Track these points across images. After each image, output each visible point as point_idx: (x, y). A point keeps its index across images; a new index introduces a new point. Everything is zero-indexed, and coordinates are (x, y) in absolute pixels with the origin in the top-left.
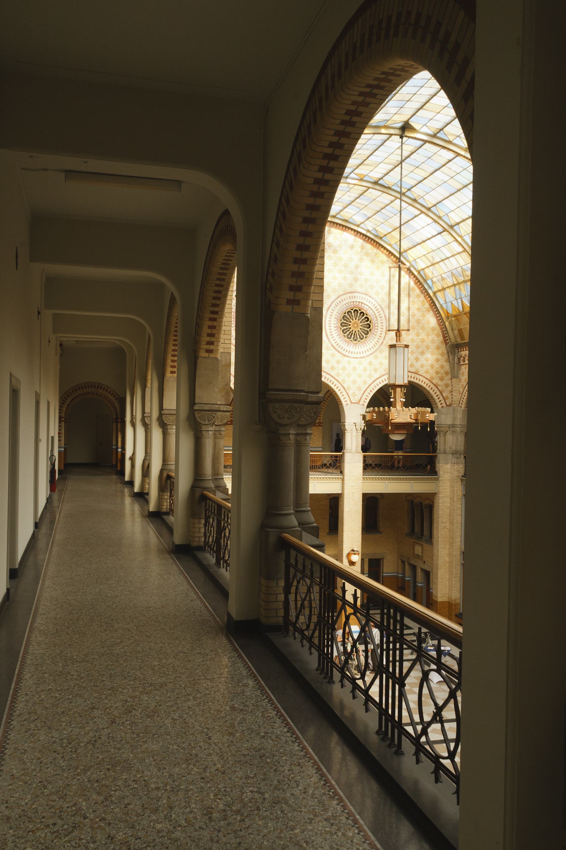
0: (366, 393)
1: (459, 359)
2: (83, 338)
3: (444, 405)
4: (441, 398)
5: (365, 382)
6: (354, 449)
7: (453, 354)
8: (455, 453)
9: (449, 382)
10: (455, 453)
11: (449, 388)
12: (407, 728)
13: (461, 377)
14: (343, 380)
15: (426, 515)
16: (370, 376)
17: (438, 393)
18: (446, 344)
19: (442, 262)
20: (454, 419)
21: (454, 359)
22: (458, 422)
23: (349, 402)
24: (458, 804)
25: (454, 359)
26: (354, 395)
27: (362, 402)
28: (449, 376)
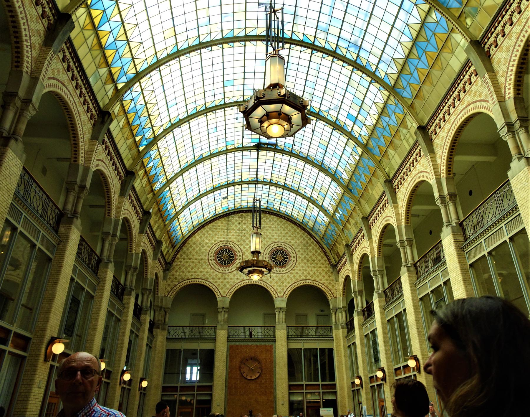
3: (332, 297)
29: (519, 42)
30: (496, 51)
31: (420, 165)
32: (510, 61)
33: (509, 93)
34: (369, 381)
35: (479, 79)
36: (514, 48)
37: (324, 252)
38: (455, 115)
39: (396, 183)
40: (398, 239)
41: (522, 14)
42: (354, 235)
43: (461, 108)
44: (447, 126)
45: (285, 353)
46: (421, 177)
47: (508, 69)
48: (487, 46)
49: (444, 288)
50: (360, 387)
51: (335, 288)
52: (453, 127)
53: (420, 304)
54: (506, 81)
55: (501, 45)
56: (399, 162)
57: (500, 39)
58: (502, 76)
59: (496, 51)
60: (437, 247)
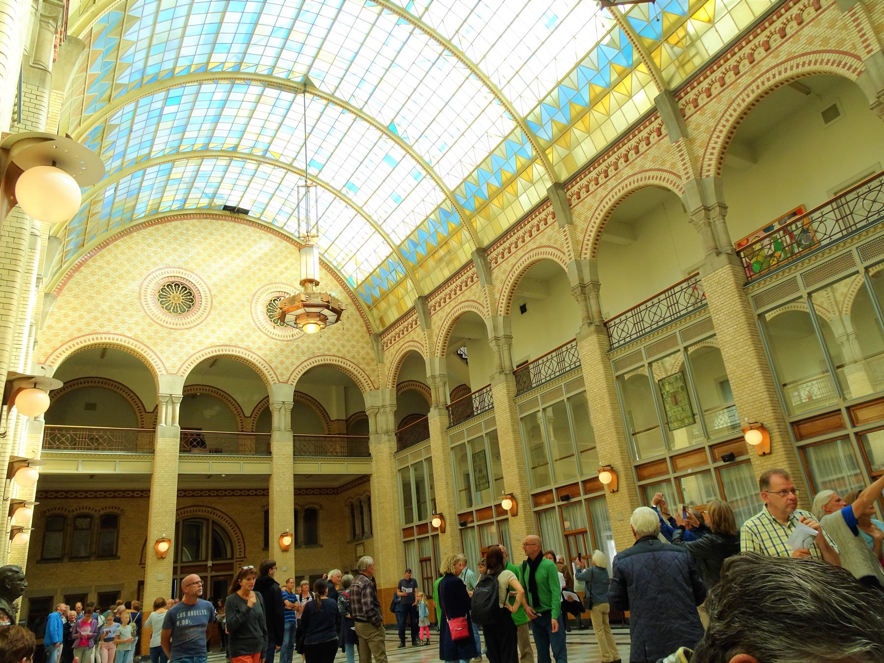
0: (294, 374)
1: (383, 346)
2: (207, 535)
3: (372, 388)
4: (369, 382)
5: (292, 364)
6: (283, 427)
7: (377, 341)
8: (387, 432)
9: (375, 368)
10: (387, 432)
11: (376, 373)
12: (628, 7)
13: (385, 361)
14: (270, 360)
15: (365, 510)
16: (298, 358)
17: (366, 377)
18: (370, 334)
19: (350, 59)
20: (384, 400)
21: (378, 346)
22: (388, 402)
23: (276, 381)
24: (226, 208)
25: (378, 346)
26: (282, 375)
27: (290, 382)
28: (375, 362)
29: (730, 111)
30: (766, 56)
31: (500, 269)
32: (714, 130)
33: (586, 254)
34: (531, 502)
35: (556, 224)
36: (723, 116)
37: (355, 304)
38: (616, 180)
39: (494, 254)
40: (428, 374)
41: (803, 27)
42: (392, 320)
43: (531, 246)
44: (601, 192)
45: (275, 447)
46: (413, 346)
47: (710, 139)
48: (683, 101)
49: (425, 464)
50: (439, 532)
51: (376, 373)
52: (610, 195)
53: (521, 427)
54: (705, 154)
55: (758, 63)
56: (397, 316)
57: (791, 27)
58: (700, 147)
59: (783, 44)
60: (481, 392)
